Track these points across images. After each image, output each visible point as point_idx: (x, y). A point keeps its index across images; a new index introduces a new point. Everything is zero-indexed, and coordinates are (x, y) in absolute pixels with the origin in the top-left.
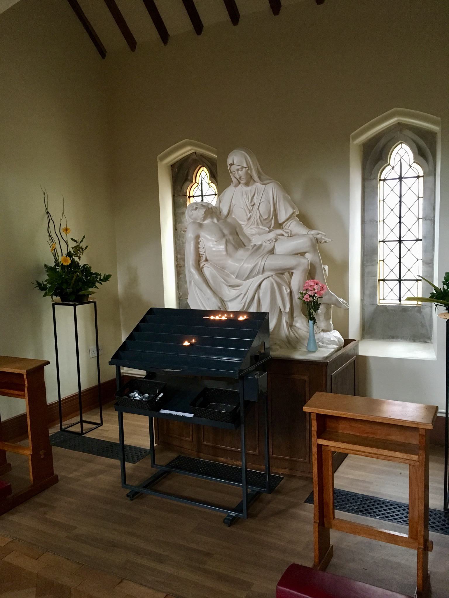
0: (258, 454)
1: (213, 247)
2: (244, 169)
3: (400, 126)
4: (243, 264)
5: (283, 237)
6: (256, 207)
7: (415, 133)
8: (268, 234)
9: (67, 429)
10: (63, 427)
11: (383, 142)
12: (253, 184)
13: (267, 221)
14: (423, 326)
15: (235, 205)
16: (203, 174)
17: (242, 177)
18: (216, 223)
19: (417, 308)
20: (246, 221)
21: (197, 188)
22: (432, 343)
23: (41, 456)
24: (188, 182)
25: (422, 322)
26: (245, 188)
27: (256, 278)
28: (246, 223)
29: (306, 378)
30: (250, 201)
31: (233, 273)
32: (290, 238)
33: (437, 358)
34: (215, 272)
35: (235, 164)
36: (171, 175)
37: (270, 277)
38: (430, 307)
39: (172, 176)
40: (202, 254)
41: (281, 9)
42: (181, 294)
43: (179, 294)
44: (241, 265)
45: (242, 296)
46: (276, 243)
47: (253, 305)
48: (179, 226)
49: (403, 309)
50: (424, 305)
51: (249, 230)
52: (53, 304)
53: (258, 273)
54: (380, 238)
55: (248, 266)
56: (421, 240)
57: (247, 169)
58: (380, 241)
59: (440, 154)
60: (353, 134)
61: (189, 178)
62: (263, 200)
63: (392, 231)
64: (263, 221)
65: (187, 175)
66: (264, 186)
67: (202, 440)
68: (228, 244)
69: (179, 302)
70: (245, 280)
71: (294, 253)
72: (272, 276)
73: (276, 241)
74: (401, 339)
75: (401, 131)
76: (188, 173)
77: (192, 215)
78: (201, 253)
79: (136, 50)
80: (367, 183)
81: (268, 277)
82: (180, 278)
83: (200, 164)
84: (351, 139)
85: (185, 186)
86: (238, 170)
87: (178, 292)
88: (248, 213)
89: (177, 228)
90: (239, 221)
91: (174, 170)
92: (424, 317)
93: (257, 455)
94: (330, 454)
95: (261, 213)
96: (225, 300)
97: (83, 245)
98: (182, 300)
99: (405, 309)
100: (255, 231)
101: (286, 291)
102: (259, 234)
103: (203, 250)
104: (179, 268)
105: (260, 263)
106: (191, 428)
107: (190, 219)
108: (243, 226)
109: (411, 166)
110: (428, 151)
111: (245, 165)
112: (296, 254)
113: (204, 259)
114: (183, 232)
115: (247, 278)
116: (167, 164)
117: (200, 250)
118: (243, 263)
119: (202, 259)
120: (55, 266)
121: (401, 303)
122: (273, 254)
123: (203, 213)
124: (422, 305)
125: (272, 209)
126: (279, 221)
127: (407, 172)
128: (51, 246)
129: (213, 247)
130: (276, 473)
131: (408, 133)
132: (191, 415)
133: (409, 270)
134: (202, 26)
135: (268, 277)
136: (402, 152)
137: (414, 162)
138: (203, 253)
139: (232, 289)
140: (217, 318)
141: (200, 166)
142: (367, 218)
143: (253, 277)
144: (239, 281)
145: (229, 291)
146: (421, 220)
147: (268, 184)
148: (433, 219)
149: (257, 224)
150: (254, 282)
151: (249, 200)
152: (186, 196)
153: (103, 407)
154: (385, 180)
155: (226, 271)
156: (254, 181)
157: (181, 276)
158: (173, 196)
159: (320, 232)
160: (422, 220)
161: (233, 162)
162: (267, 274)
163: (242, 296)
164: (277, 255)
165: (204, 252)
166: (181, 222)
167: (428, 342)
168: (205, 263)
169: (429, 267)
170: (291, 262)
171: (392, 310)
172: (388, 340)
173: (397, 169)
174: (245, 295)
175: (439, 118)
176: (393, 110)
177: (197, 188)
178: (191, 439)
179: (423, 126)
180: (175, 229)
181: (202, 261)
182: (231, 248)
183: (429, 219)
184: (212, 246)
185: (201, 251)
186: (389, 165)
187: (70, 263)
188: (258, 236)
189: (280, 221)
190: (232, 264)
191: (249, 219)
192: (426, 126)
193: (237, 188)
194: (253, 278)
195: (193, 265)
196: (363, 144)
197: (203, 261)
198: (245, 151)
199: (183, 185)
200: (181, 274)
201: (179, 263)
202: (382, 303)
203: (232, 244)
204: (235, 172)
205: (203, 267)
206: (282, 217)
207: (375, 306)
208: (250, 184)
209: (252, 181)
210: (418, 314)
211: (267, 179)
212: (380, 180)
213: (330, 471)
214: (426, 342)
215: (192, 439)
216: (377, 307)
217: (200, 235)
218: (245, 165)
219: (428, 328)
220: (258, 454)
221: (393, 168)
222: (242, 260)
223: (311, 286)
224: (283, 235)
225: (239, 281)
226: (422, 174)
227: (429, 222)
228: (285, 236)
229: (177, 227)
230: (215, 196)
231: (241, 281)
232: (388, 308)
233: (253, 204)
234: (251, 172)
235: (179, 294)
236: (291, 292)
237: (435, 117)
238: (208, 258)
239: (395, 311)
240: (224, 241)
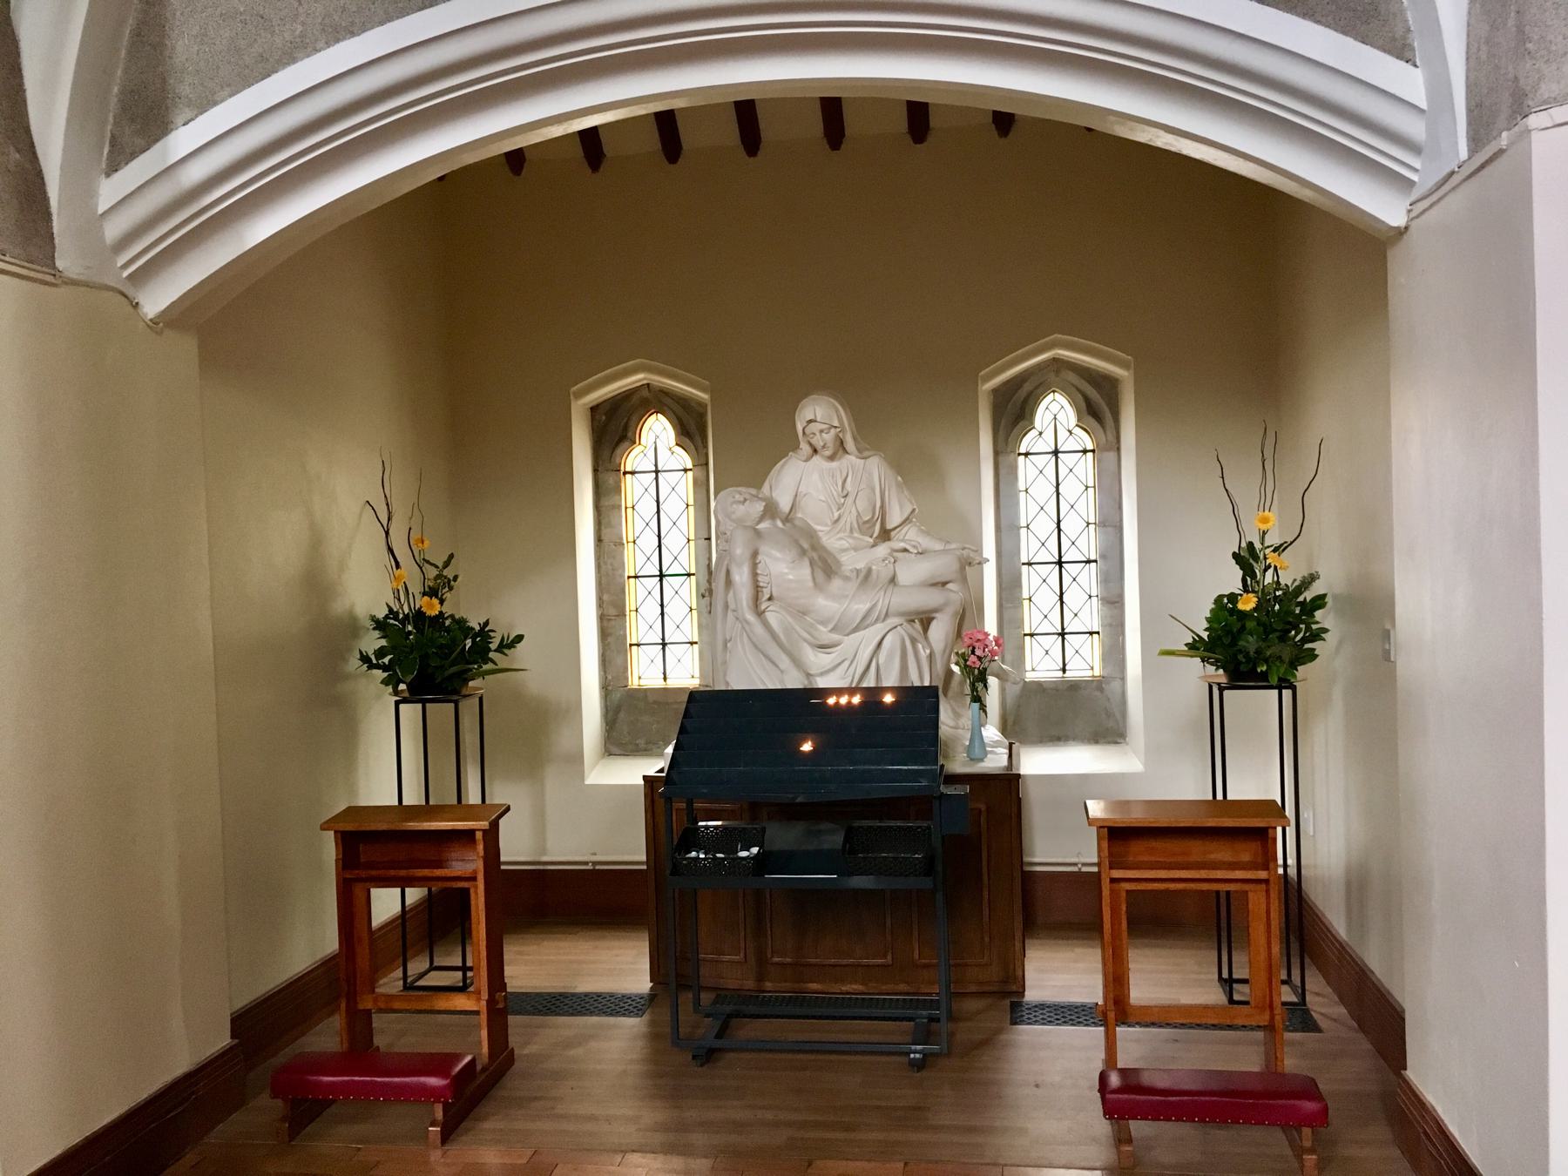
1: (787, 574)
2: (833, 430)
6: (850, 500)
7: (1082, 376)
9: (418, 984)
11: (1027, 387)
13: (867, 525)
14: (1109, 715)
15: (805, 495)
16: (657, 430)
17: (828, 445)
18: (782, 529)
19: (1095, 683)
20: (830, 523)
21: (642, 455)
22: (1127, 744)
23: (498, 1003)
24: (626, 444)
25: (1106, 708)
27: (872, 629)
28: (828, 529)
29: (983, 807)
30: (840, 489)
31: (823, 623)
32: (918, 556)
33: (1145, 767)
36: (590, 428)
38: (1120, 679)
39: (593, 429)
40: (762, 587)
42: (610, 677)
45: (846, 664)
47: (868, 678)
48: (606, 533)
49: (1071, 685)
50: (1107, 677)
52: (395, 701)
53: (877, 621)
54: (630, 571)
56: (1024, 564)
57: (838, 430)
58: (629, 577)
60: (982, 373)
61: (630, 434)
62: (862, 486)
63: (1043, 544)
64: (864, 526)
65: (626, 428)
66: (863, 461)
68: (815, 567)
69: (606, 696)
70: (848, 635)
72: (901, 625)
75: (1057, 372)
76: (627, 422)
77: (734, 513)
81: (896, 627)
84: (980, 382)
85: (618, 451)
86: (821, 431)
87: (602, 673)
88: (834, 510)
89: (603, 538)
94: (1124, 894)
99: (1074, 687)
101: (924, 653)
102: (856, 549)
104: (605, 624)
107: (727, 520)
108: (820, 534)
109: (1070, 432)
112: (934, 585)
113: (768, 596)
115: (855, 630)
116: (585, 404)
118: (847, 603)
119: (763, 596)
120: (387, 617)
121: (1065, 675)
122: (895, 584)
123: (762, 509)
124: (1103, 677)
125: (878, 505)
127: (1067, 444)
130: (927, 994)
131: (1072, 377)
133: (1076, 615)
135: (896, 627)
136: (1055, 408)
137: (677, 444)
138: (765, 585)
140: (844, 700)
141: (653, 411)
143: (865, 628)
144: (835, 637)
145: (816, 655)
146: (1092, 527)
147: (869, 457)
148: (1118, 524)
149: (851, 530)
151: (837, 485)
152: (619, 471)
153: (435, 949)
156: (846, 452)
157: (610, 639)
158: (596, 471)
159: (967, 546)
160: (1022, 525)
161: (816, 416)
163: (846, 664)
165: (768, 583)
166: (609, 525)
169: (1115, 608)
171: (1051, 689)
173: (1049, 435)
174: (852, 662)
176: (1052, 337)
177: (642, 455)
179: (1084, 361)
180: (599, 540)
182: (820, 576)
183: (1110, 523)
184: (786, 571)
186: (1034, 428)
187: (425, 613)
188: (853, 553)
189: (889, 526)
190: (824, 604)
193: (808, 463)
196: (992, 390)
197: (766, 601)
198: (834, 399)
200: (610, 635)
202: (1030, 676)
203: (820, 567)
206: (894, 519)
207: (1022, 684)
208: (838, 456)
209: (841, 452)
210: (1098, 693)
211: (867, 449)
213: (1123, 925)
214: (1116, 743)
215: (745, 957)
217: (760, 551)
219: (1118, 715)
221: (1041, 433)
222: (847, 596)
224: (905, 550)
225: (835, 637)
226: (690, 465)
228: (911, 553)
230: (683, 472)
231: (840, 637)
233: (845, 493)
236: (931, 657)
238: (774, 594)
239: (1057, 690)
240: (806, 563)
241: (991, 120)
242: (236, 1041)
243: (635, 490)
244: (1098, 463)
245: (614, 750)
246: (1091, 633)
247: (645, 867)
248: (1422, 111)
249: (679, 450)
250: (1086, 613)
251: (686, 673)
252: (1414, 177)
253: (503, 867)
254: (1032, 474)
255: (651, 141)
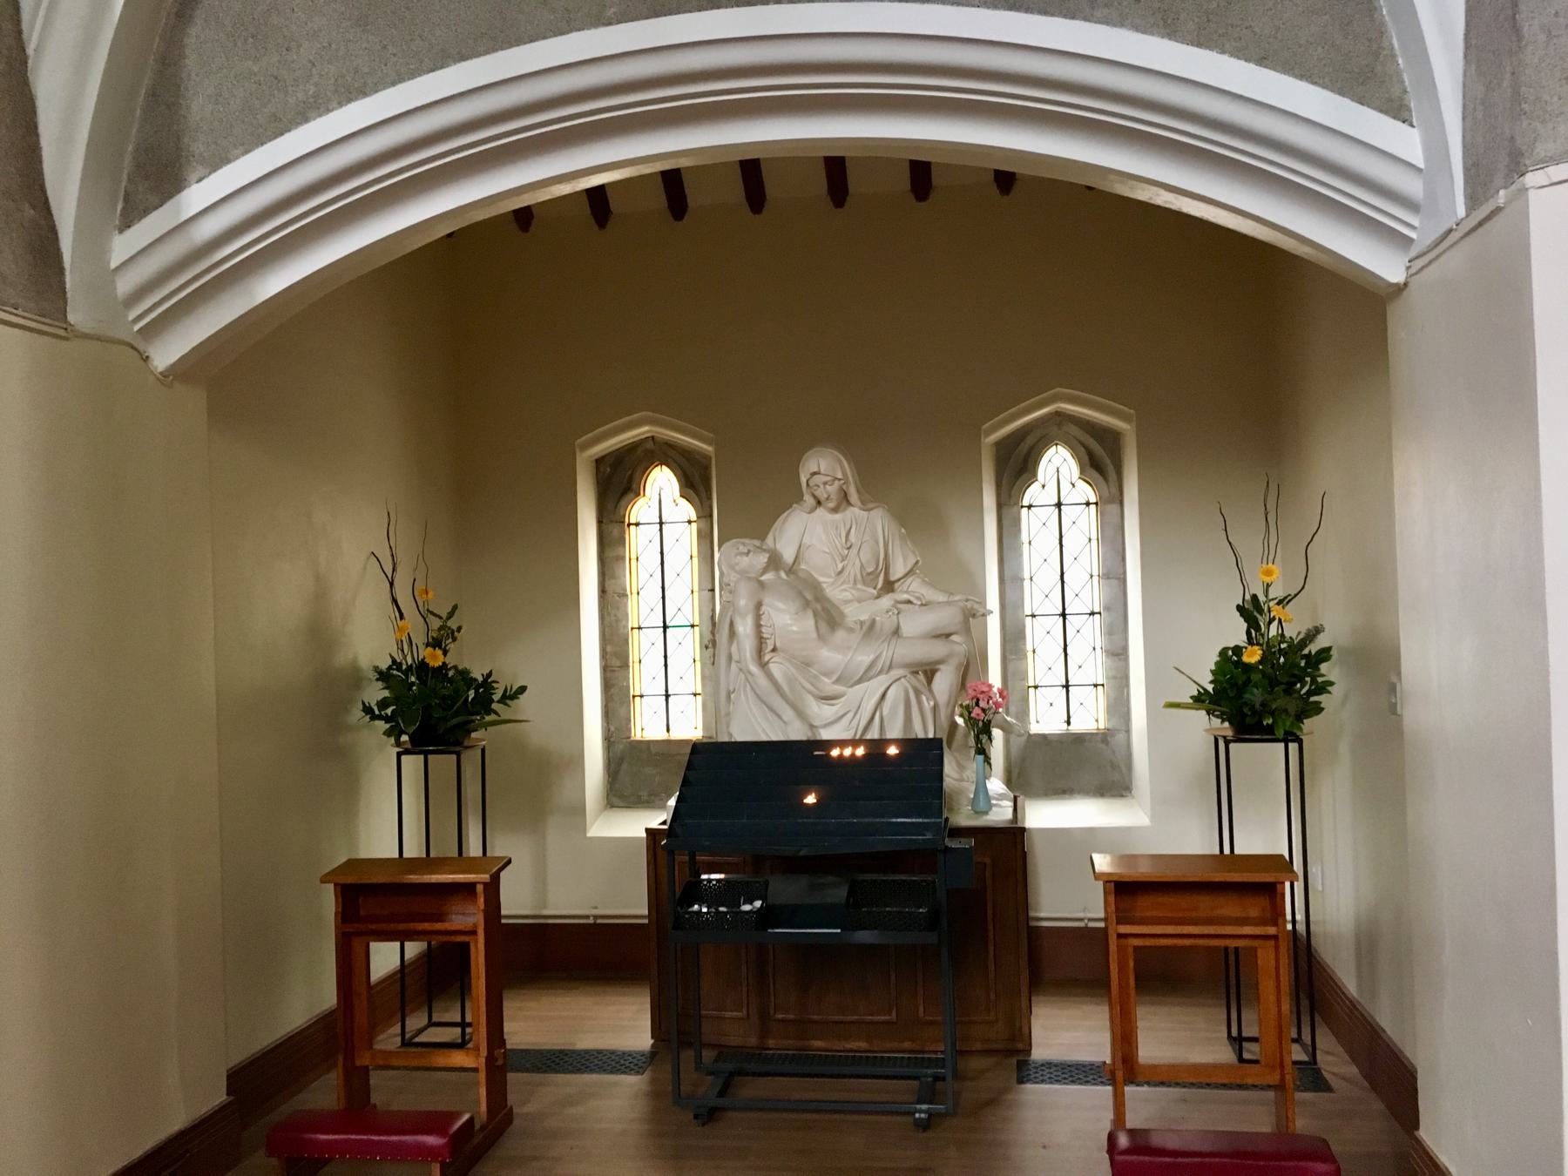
0: (895, 1020)
2: (837, 482)
3: (1060, 418)
4: (852, 656)
5: (910, 606)
6: (854, 551)
8: (877, 601)
10: (407, 1036)
11: (1029, 441)
12: (845, 509)
13: (871, 577)
14: (1114, 767)
17: (832, 496)
19: (1100, 736)
20: (833, 575)
23: (497, 1060)
26: (830, 516)
28: (831, 580)
29: (988, 861)
31: (827, 674)
33: (1152, 822)
34: (794, 671)
35: (822, 471)
37: (903, 680)
39: (598, 482)
41: (848, 198)
42: (612, 729)
43: (609, 730)
44: (848, 658)
45: (850, 715)
46: (900, 616)
51: (837, 593)
53: (880, 672)
55: (864, 659)
57: (842, 482)
59: (1136, 469)
60: (987, 425)
61: (634, 486)
64: (868, 578)
67: (772, 1012)
70: (852, 686)
71: (933, 634)
72: (905, 677)
73: (898, 613)
74: (1079, 793)
75: (1059, 425)
78: (765, 636)
79: (532, 229)
80: (1005, 510)
81: (899, 679)
82: (612, 695)
83: (658, 460)
86: (825, 483)
88: (838, 562)
89: (607, 588)
90: (816, 576)
91: (602, 470)
92: (1114, 752)
93: (893, 1023)
95: (863, 561)
96: (815, 724)
97: (452, 624)
98: (614, 742)
99: (1079, 739)
100: (853, 595)
101: (928, 705)
102: (859, 601)
103: (770, 630)
104: (608, 675)
105: (885, 653)
106: (745, 989)
108: (825, 586)
109: (1073, 485)
110: (1108, 461)
111: (840, 475)
113: (772, 647)
114: (617, 598)
115: (859, 681)
116: (591, 457)
117: (763, 630)
120: (390, 668)
122: (899, 636)
126: (891, 575)
128: (396, 627)
129: (791, 625)
130: (930, 1052)
131: (1073, 429)
132: (839, 931)
134: (687, 206)
135: (899, 679)
136: (1057, 461)
139: (823, 703)
140: (847, 752)
142: (1007, 574)
145: (819, 707)
147: (872, 509)
150: (875, 687)
152: (624, 522)
154: (1030, 507)
155: (812, 670)
156: (849, 503)
158: (600, 522)
159: (972, 598)
162: (896, 673)
163: (850, 715)
164: (907, 638)
166: (613, 577)
167: (1126, 796)
168: (772, 654)
170: (937, 650)
172: (1057, 796)
175: (1132, 411)
178: (745, 1012)
180: (603, 591)
181: (767, 651)
183: (1114, 575)
184: (789, 622)
185: (766, 631)
188: (856, 604)
190: (830, 656)
191: (840, 573)
192: (1102, 420)
194: (869, 680)
195: (753, 659)
199: (618, 502)
200: (613, 686)
201: (609, 661)
202: (1035, 729)
204: (818, 486)
205: (767, 663)
206: (898, 569)
207: (1024, 739)
208: (841, 509)
209: (845, 503)
210: (1103, 746)
212: (1022, 507)
214: (1122, 796)
215: (748, 1014)
216: (1028, 737)
217: (764, 603)
218: (840, 475)
220: (895, 1020)
223: (983, 692)
224: (909, 602)
225: (840, 688)
226: (1093, 499)
227: (1114, 582)
228: (915, 605)
229: (606, 585)
232: (1049, 737)
234: (848, 487)
235: (609, 730)
237: (1126, 408)
240: (810, 613)
241: (826, 193)
242: (231, 1098)
243: (640, 542)
244: (1102, 515)
245: (615, 801)
246: (1096, 686)
247: (646, 921)
248: (1419, 170)
249: (1082, 485)
250: (1090, 665)
251: (689, 726)
252: (1413, 235)
253: (503, 921)
254: (1036, 524)
255: (659, 200)
